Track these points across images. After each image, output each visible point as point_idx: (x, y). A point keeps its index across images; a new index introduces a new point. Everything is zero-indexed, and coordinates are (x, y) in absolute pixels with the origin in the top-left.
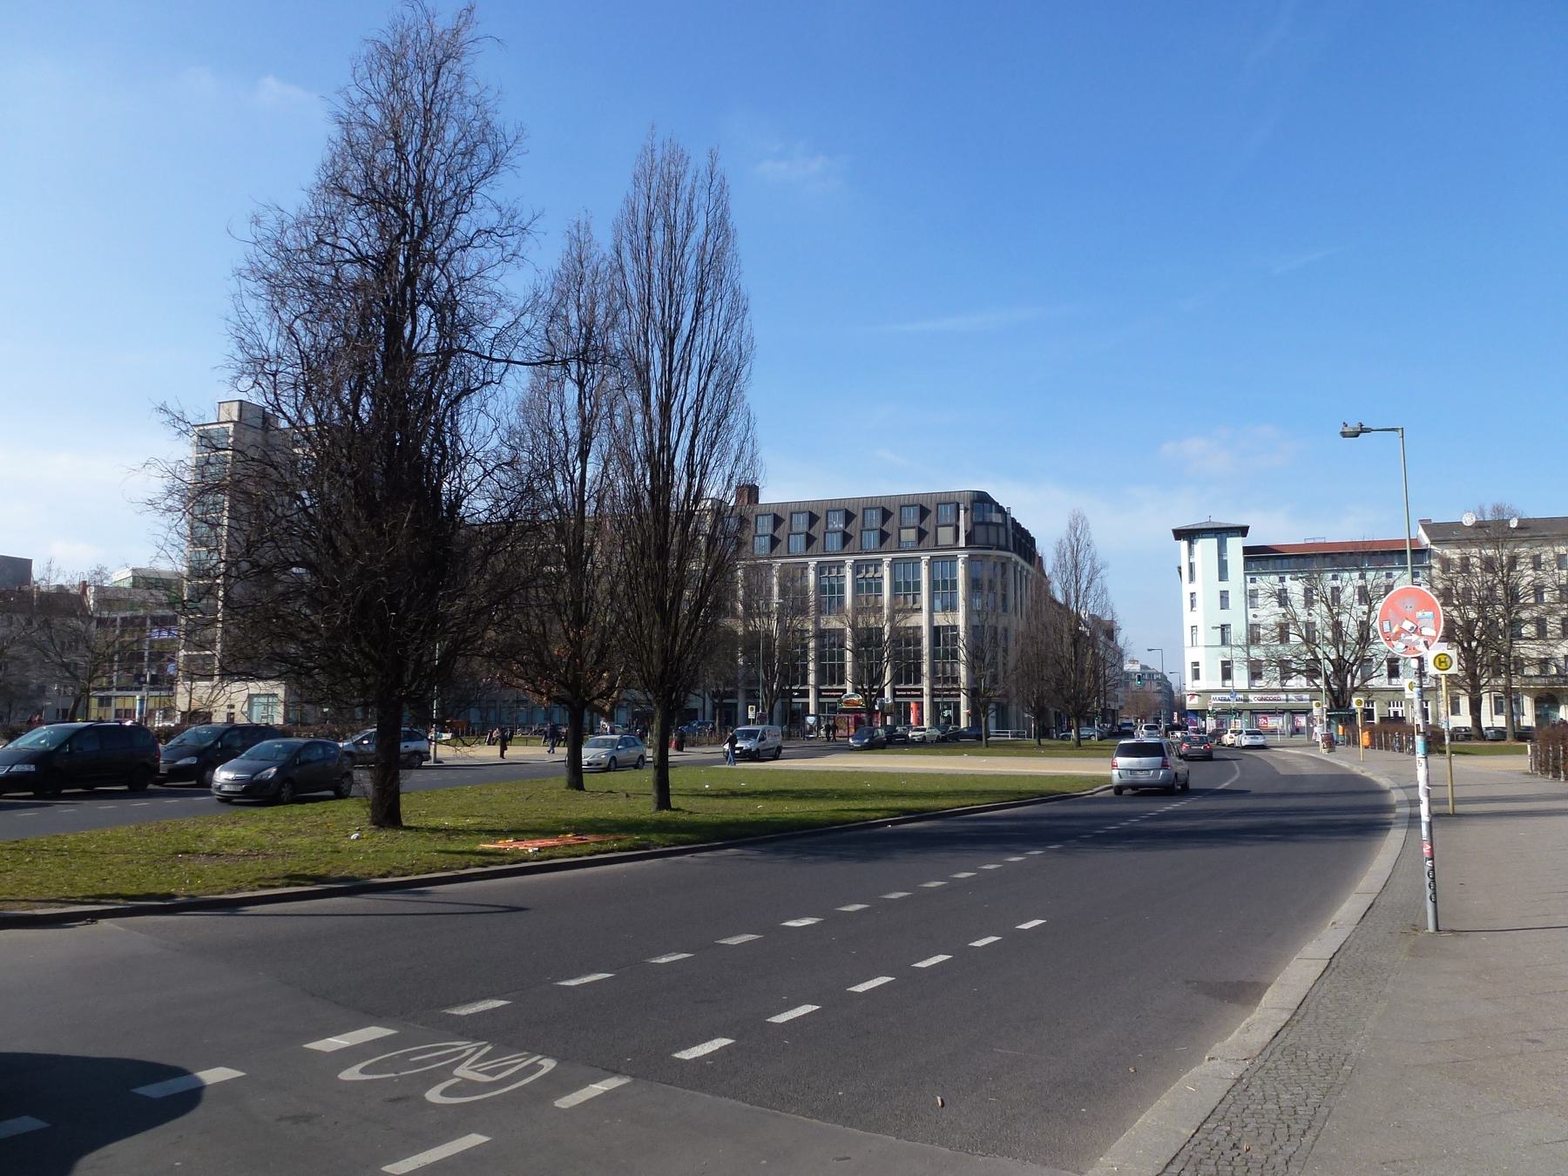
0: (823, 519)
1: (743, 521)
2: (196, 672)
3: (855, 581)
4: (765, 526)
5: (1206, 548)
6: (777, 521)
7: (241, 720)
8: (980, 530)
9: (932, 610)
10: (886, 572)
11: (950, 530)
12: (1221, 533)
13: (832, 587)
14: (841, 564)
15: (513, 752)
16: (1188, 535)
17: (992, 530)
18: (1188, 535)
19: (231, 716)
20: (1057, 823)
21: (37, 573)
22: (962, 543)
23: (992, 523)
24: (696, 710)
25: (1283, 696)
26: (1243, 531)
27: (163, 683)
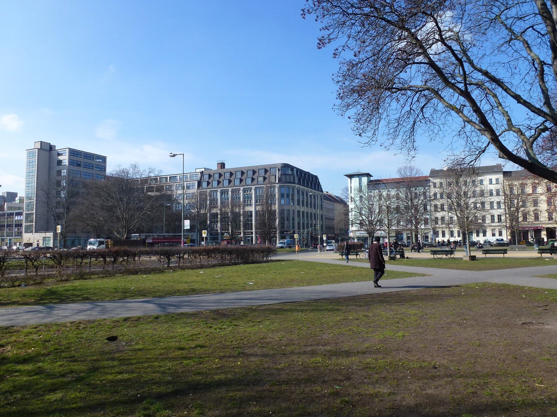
0: (257, 173)
1: (220, 175)
2: (29, 230)
3: (244, 195)
4: (228, 175)
5: (356, 180)
6: (231, 174)
7: (41, 245)
8: (284, 177)
9: (256, 205)
10: (253, 191)
11: (273, 177)
12: (360, 175)
13: (248, 196)
14: (217, 191)
15: (358, 257)
16: (351, 176)
17: (288, 177)
18: (351, 176)
19: (38, 245)
20: (404, 289)
21: (111, 169)
22: (277, 181)
23: (289, 175)
24: (194, 240)
25: (380, 232)
26: (368, 175)
27: (20, 234)
